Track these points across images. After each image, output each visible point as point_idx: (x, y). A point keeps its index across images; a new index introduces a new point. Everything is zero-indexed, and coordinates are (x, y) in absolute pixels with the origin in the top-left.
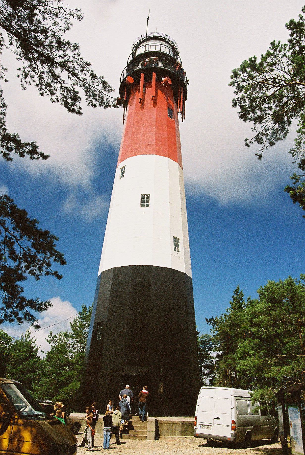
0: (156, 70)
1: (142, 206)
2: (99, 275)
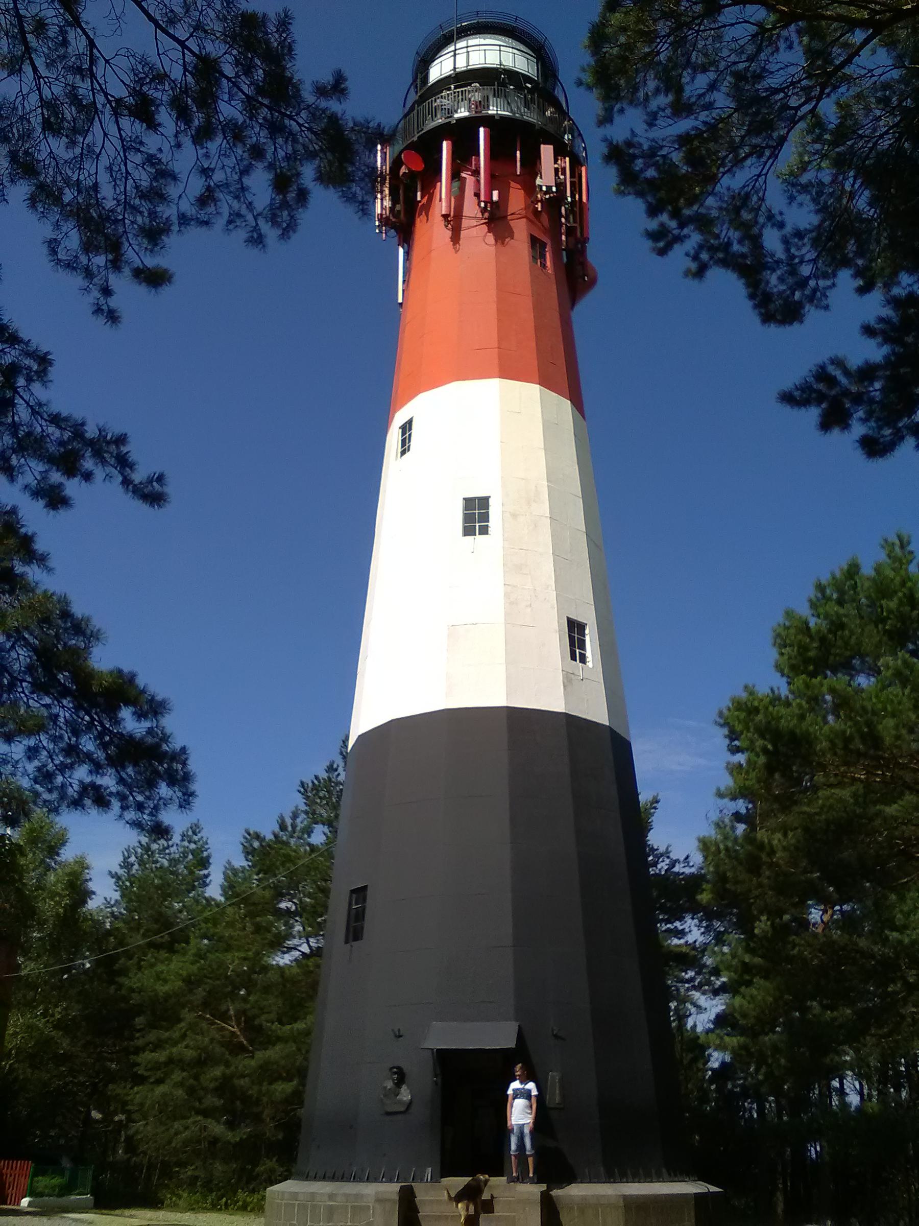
0: (489, 121)
1: (468, 531)
2: (713, 1189)
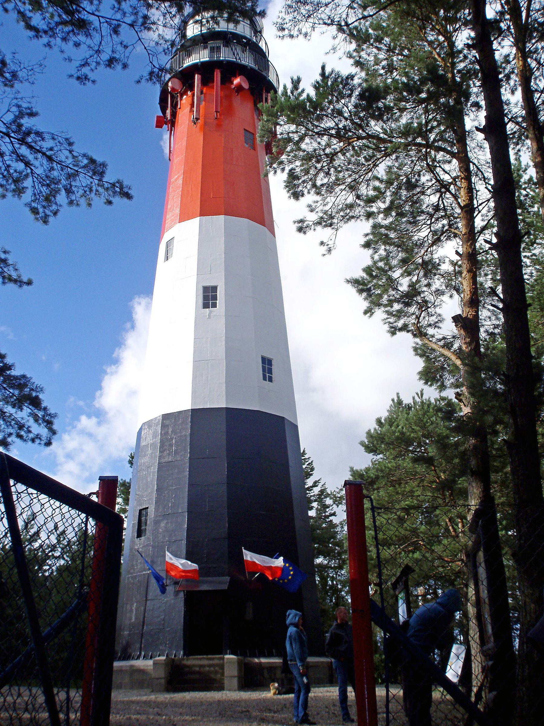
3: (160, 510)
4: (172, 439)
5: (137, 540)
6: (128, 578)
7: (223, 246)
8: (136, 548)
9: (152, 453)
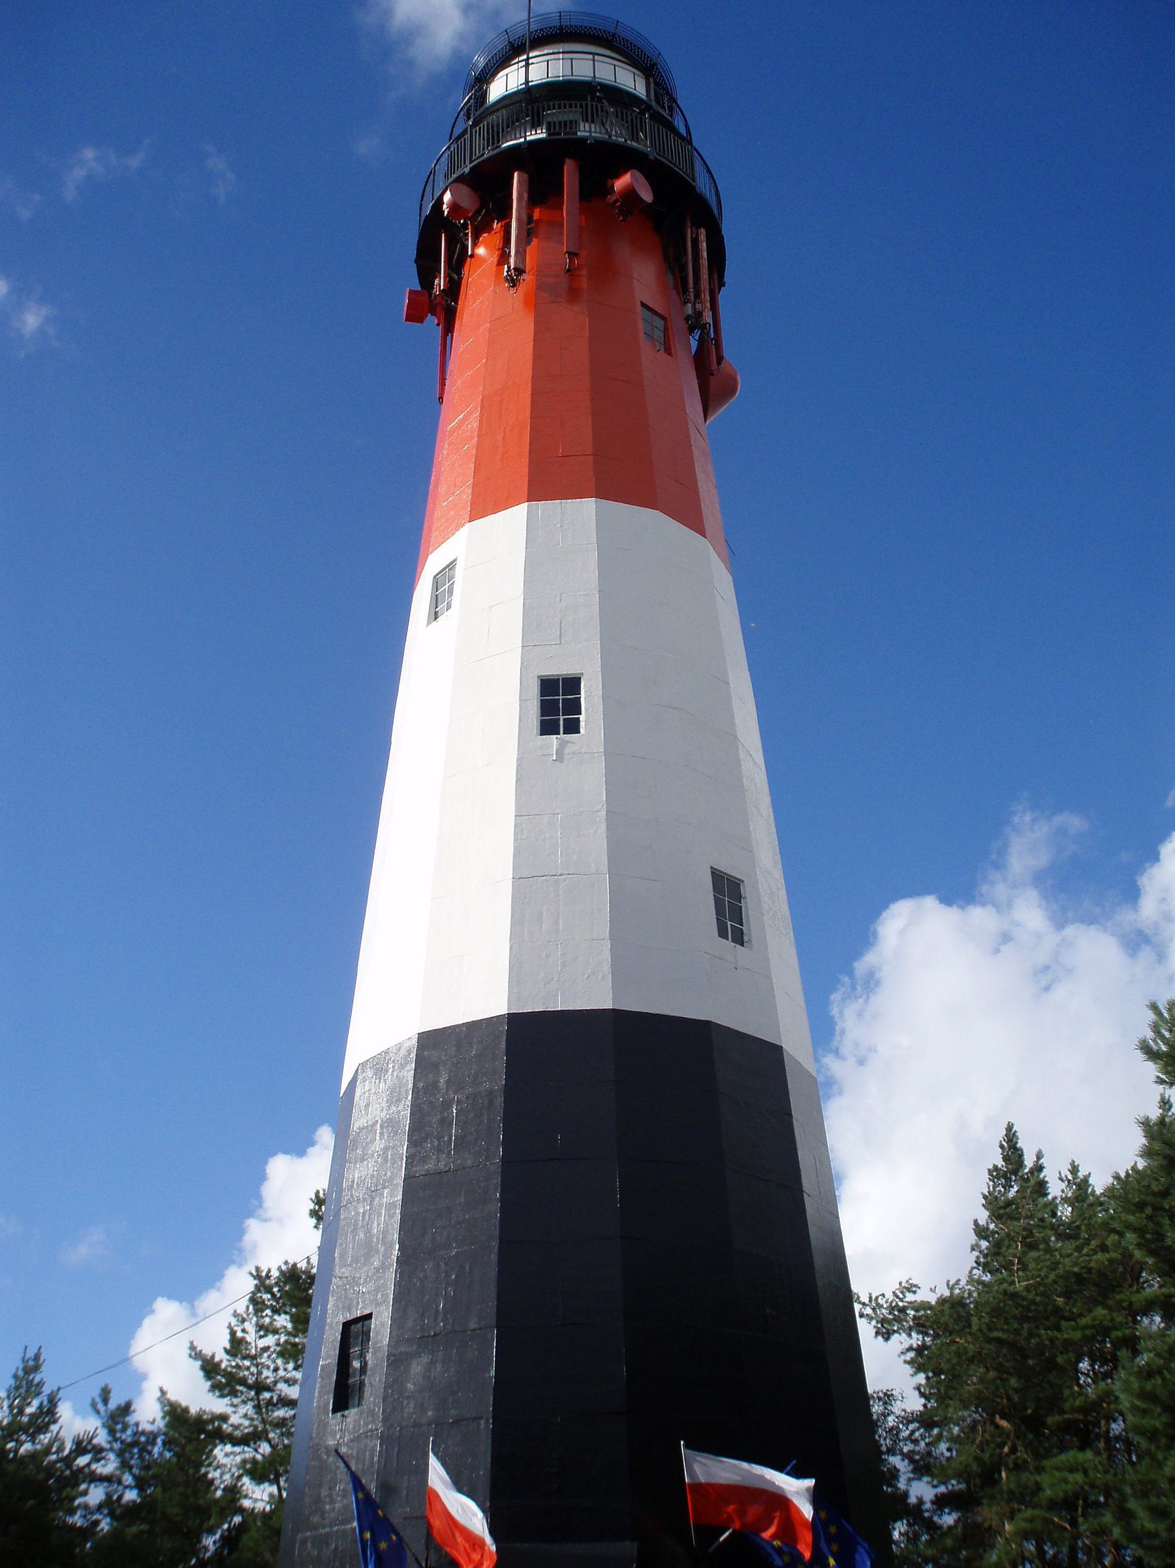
0: (577, 148)
1: (548, 728)
3: (410, 1323)
4: (447, 1105)
5: (334, 1421)
6: (304, 1542)
7: (594, 573)
8: (331, 1442)
9: (386, 1149)
